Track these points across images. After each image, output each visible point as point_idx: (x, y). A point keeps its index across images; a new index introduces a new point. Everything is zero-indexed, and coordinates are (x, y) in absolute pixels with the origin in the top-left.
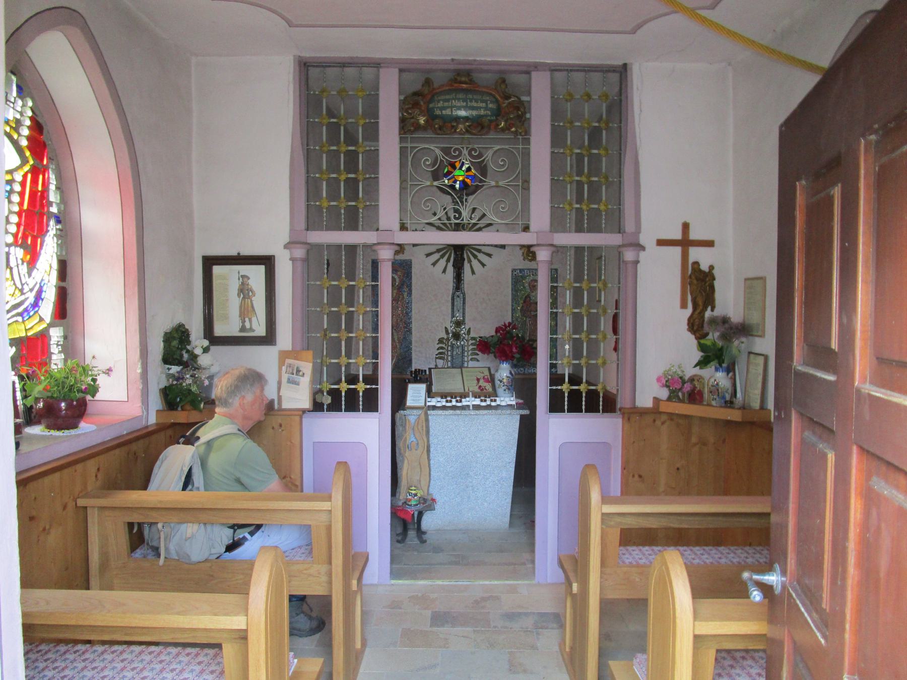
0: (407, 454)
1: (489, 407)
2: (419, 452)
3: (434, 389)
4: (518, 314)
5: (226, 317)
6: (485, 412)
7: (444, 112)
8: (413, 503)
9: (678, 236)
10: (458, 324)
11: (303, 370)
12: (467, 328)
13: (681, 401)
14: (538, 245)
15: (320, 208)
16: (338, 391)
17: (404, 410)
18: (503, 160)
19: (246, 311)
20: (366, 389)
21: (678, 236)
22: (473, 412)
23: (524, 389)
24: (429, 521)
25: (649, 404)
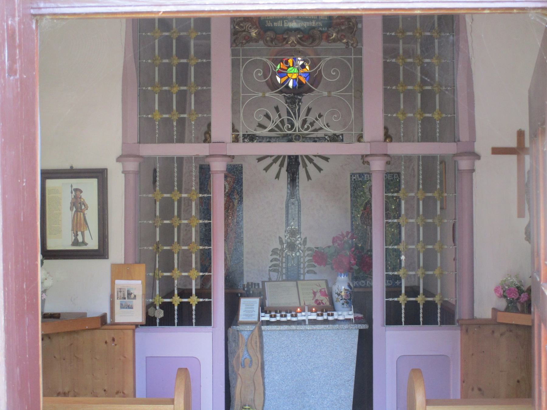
1: (326, 322)
2: (253, 369)
4: (359, 222)
6: (322, 327)
9: (513, 143)
10: (293, 233)
12: (303, 237)
13: (517, 311)
14: (371, 155)
16: (171, 305)
17: (237, 325)
18: (334, 71)
21: (513, 143)
22: (309, 327)
23: (360, 302)
25: (488, 315)
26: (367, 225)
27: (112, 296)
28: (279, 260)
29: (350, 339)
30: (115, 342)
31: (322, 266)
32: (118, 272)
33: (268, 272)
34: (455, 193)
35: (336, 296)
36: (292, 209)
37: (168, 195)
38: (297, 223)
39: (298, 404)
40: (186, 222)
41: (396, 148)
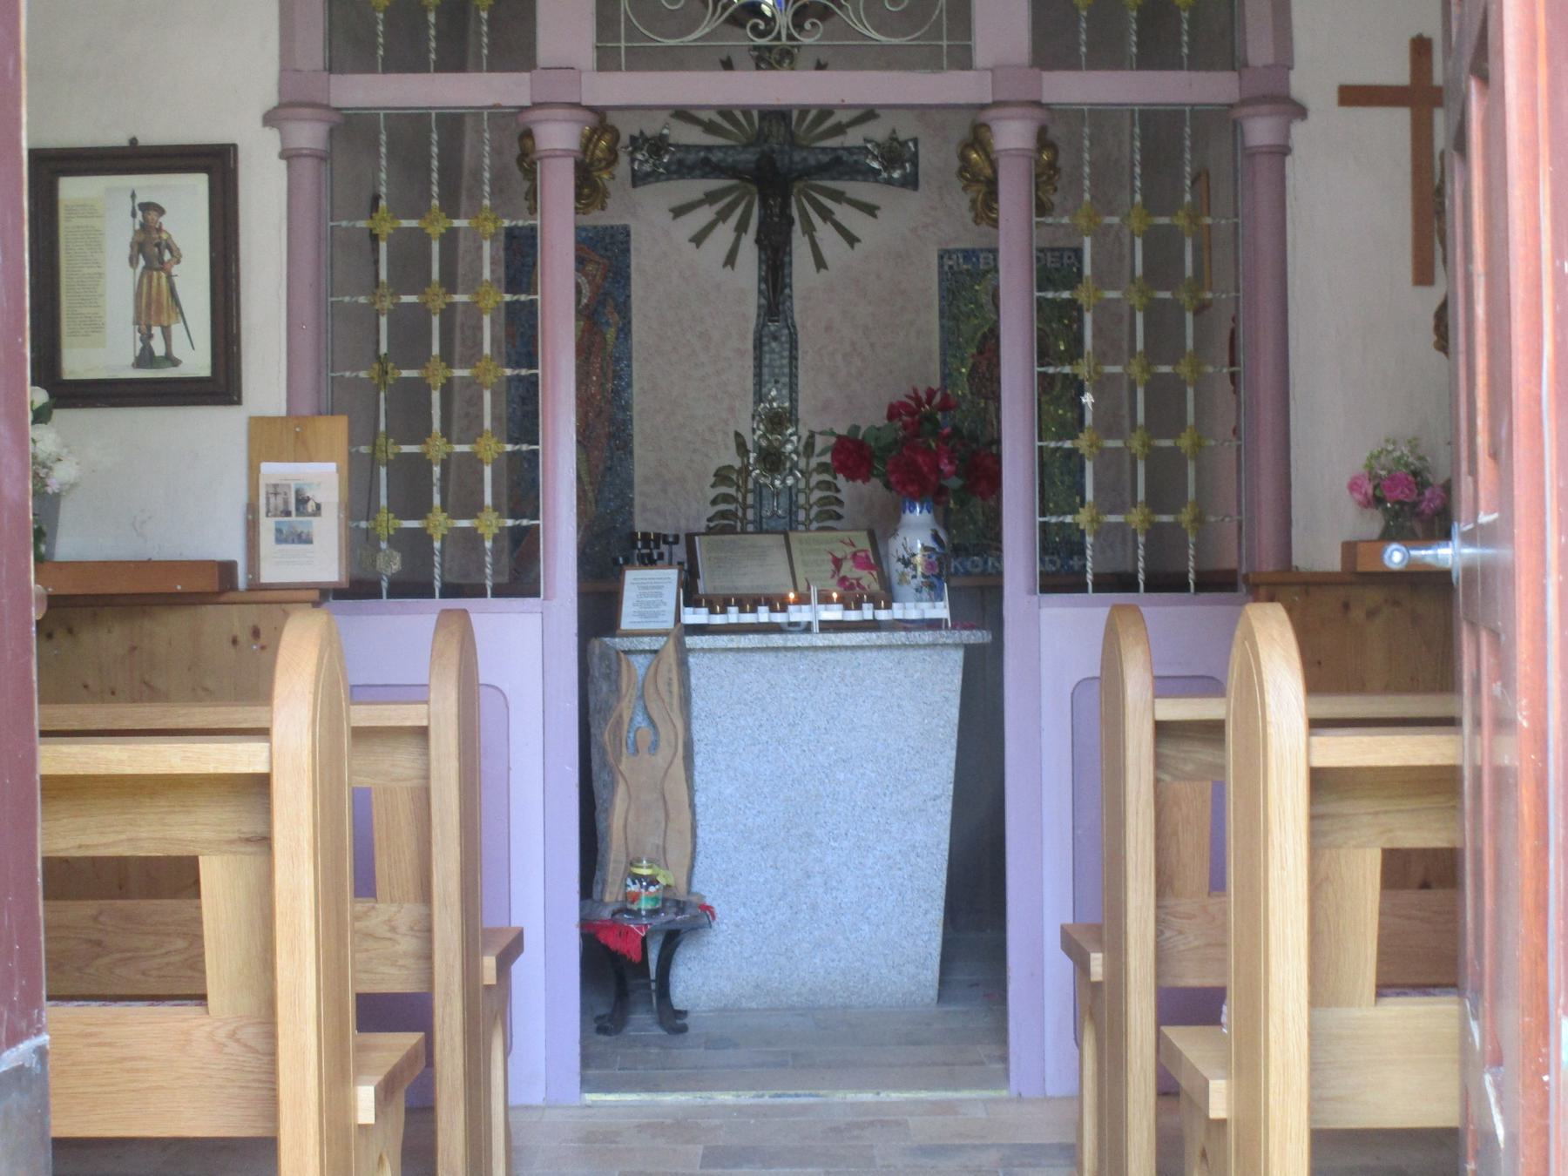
0: (624, 766)
2: (661, 759)
3: (703, 586)
5: (95, 326)
8: (644, 905)
9: (1397, 73)
10: (777, 421)
12: (804, 434)
17: (613, 635)
19: (155, 306)
21: (1397, 73)
24: (697, 980)
25: (1331, 561)
26: (987, 398)
27: (252, 508)
28: (735, 500)
29: (939, 678)
30: (263, 640)
31: (859, 482)
32: (268, 439)
34: (1236, 216)
35: (900, 566)
36: (772, 351)
37: (413, 223)
38: (785, 392)
39: (792, 867)
40: (465, 373)
41: (1072, 88)
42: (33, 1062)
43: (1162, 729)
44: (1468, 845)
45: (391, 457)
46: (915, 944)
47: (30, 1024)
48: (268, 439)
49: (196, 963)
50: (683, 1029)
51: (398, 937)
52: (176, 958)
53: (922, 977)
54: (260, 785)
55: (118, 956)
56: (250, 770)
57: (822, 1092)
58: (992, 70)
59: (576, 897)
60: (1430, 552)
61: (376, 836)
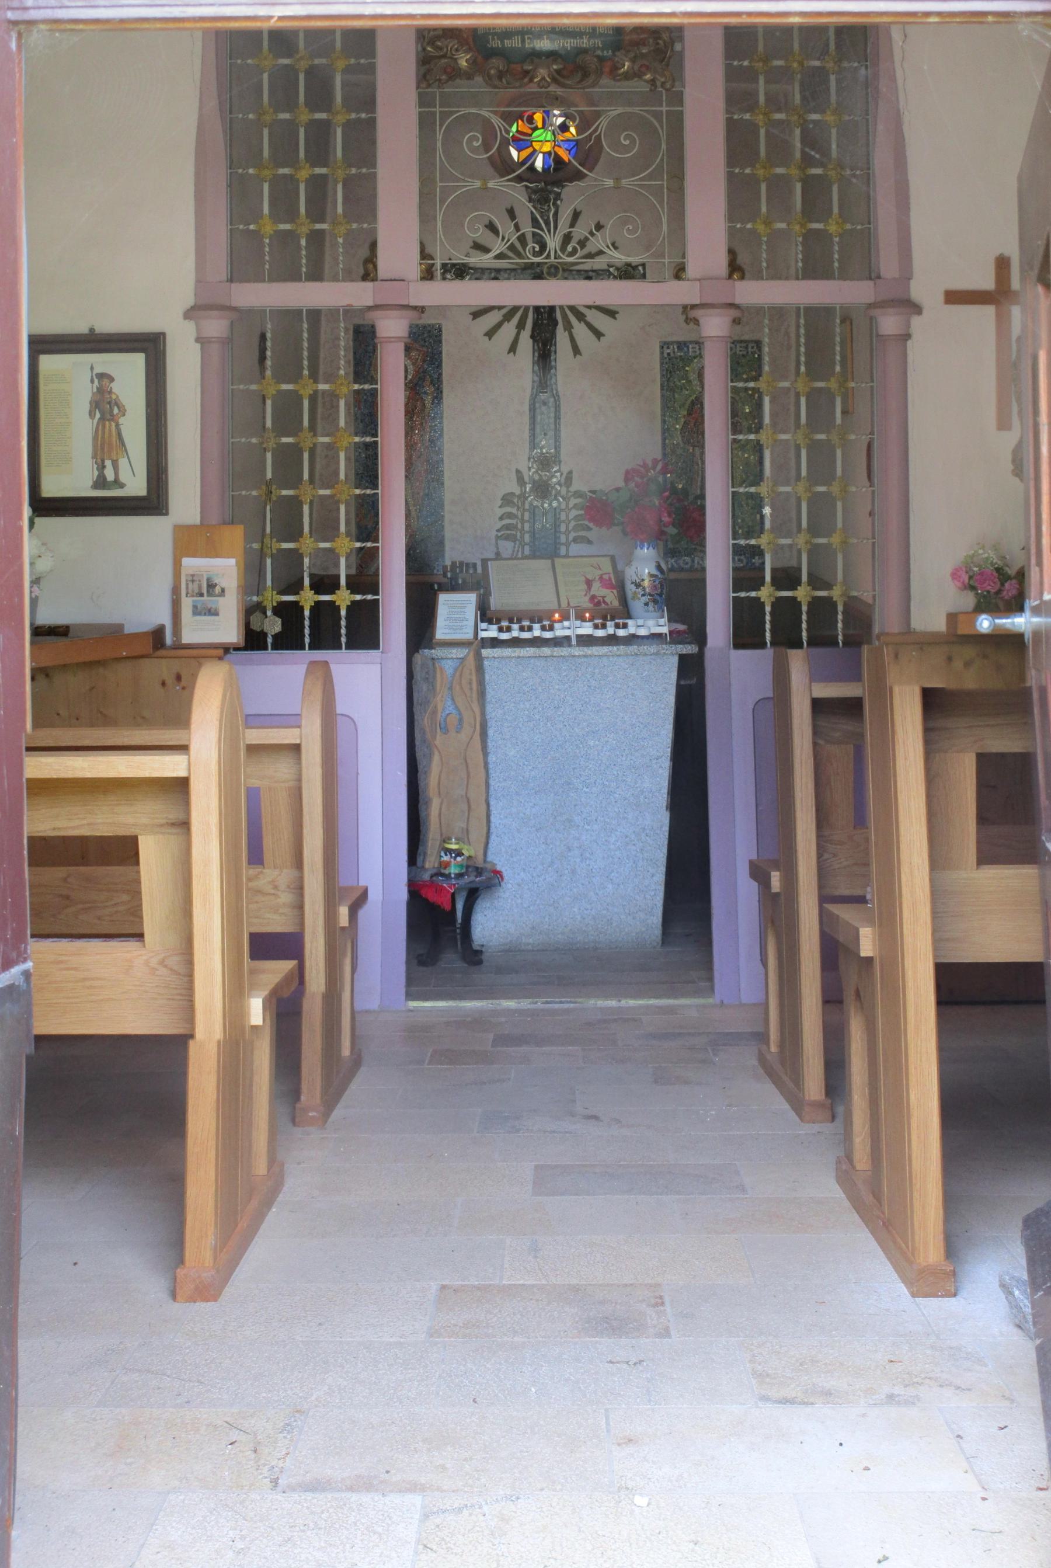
0: (439, 740)
1: (612, 640)
2: (463, 736)
4: (677, 440)
7: (507, 43)
8: (453, 870)
9: (987, 282)
10: (545, 462)
11: (222, 582)
12: (565, 470)
15: (257, 235)
16: (297, 607)
20: (353, 602)
21: (987, 282)
22: (577, 651)
24: (491, 924)
26: (694, 446)
27: (176, 591)
28: (516, 517)
30: (183, 683)
32: (188, 541)
33: (493, 541)
34: (873, 381)
36: (542, 414)
37: (290, 387)
38: (552, 441)
39: (558, 843)
41: (752, 292)
42: (21, 981)
43: (818, 706)
44: (1039, 752)
45: (274, 551)
46: (645, 898)
47: (19, 955)
48: (188, 541)
49: (136, 912)
50: (480, 962)
51: (279, 893)
52: (122, 908)
53: (649, 921)
54: (181, 786)
55: (81, 906)
56: (175, 775)
57: (580, 1000)
58: (699, 280)
59: (406, 865)
60: (1009, 621)
61: (264, 821)
